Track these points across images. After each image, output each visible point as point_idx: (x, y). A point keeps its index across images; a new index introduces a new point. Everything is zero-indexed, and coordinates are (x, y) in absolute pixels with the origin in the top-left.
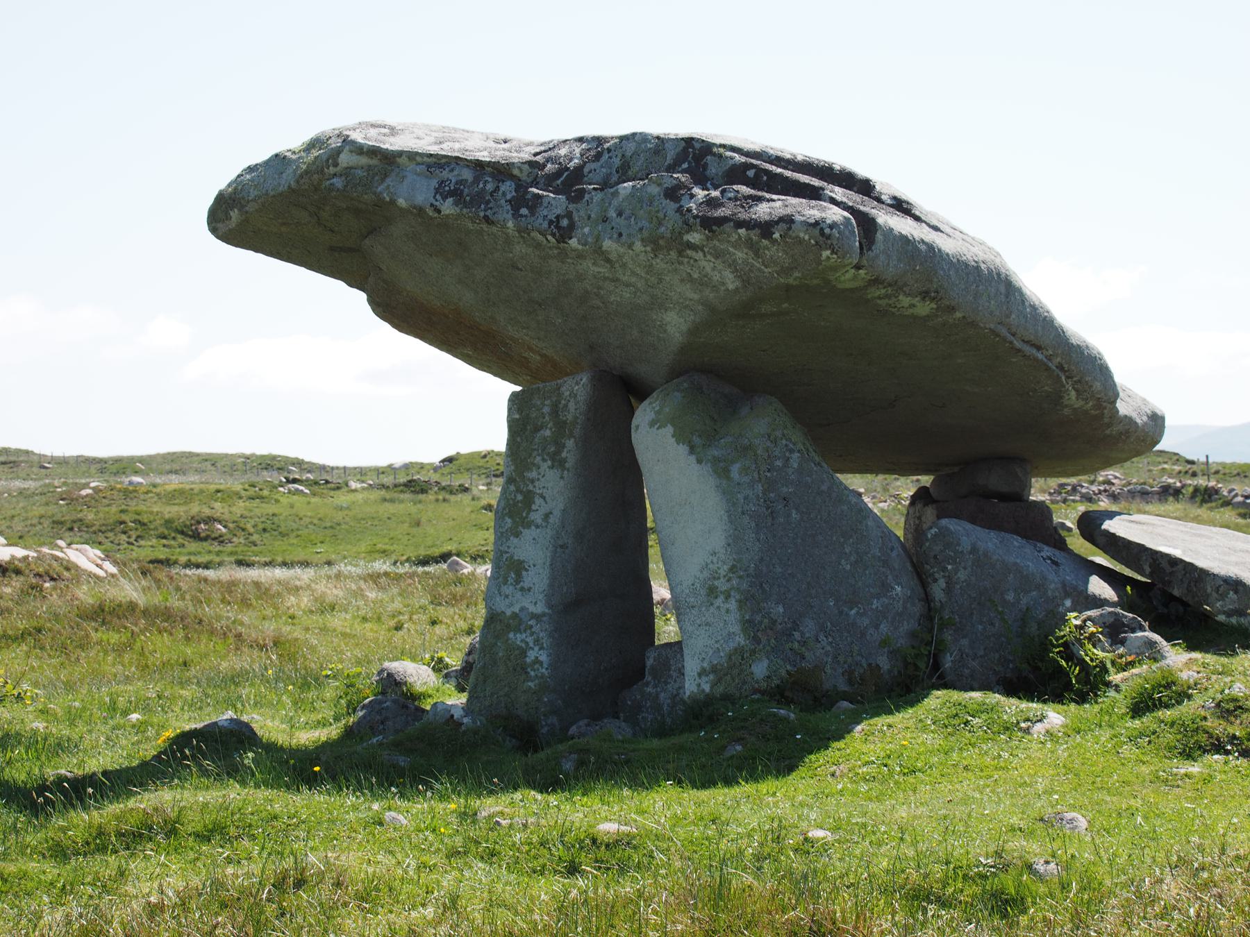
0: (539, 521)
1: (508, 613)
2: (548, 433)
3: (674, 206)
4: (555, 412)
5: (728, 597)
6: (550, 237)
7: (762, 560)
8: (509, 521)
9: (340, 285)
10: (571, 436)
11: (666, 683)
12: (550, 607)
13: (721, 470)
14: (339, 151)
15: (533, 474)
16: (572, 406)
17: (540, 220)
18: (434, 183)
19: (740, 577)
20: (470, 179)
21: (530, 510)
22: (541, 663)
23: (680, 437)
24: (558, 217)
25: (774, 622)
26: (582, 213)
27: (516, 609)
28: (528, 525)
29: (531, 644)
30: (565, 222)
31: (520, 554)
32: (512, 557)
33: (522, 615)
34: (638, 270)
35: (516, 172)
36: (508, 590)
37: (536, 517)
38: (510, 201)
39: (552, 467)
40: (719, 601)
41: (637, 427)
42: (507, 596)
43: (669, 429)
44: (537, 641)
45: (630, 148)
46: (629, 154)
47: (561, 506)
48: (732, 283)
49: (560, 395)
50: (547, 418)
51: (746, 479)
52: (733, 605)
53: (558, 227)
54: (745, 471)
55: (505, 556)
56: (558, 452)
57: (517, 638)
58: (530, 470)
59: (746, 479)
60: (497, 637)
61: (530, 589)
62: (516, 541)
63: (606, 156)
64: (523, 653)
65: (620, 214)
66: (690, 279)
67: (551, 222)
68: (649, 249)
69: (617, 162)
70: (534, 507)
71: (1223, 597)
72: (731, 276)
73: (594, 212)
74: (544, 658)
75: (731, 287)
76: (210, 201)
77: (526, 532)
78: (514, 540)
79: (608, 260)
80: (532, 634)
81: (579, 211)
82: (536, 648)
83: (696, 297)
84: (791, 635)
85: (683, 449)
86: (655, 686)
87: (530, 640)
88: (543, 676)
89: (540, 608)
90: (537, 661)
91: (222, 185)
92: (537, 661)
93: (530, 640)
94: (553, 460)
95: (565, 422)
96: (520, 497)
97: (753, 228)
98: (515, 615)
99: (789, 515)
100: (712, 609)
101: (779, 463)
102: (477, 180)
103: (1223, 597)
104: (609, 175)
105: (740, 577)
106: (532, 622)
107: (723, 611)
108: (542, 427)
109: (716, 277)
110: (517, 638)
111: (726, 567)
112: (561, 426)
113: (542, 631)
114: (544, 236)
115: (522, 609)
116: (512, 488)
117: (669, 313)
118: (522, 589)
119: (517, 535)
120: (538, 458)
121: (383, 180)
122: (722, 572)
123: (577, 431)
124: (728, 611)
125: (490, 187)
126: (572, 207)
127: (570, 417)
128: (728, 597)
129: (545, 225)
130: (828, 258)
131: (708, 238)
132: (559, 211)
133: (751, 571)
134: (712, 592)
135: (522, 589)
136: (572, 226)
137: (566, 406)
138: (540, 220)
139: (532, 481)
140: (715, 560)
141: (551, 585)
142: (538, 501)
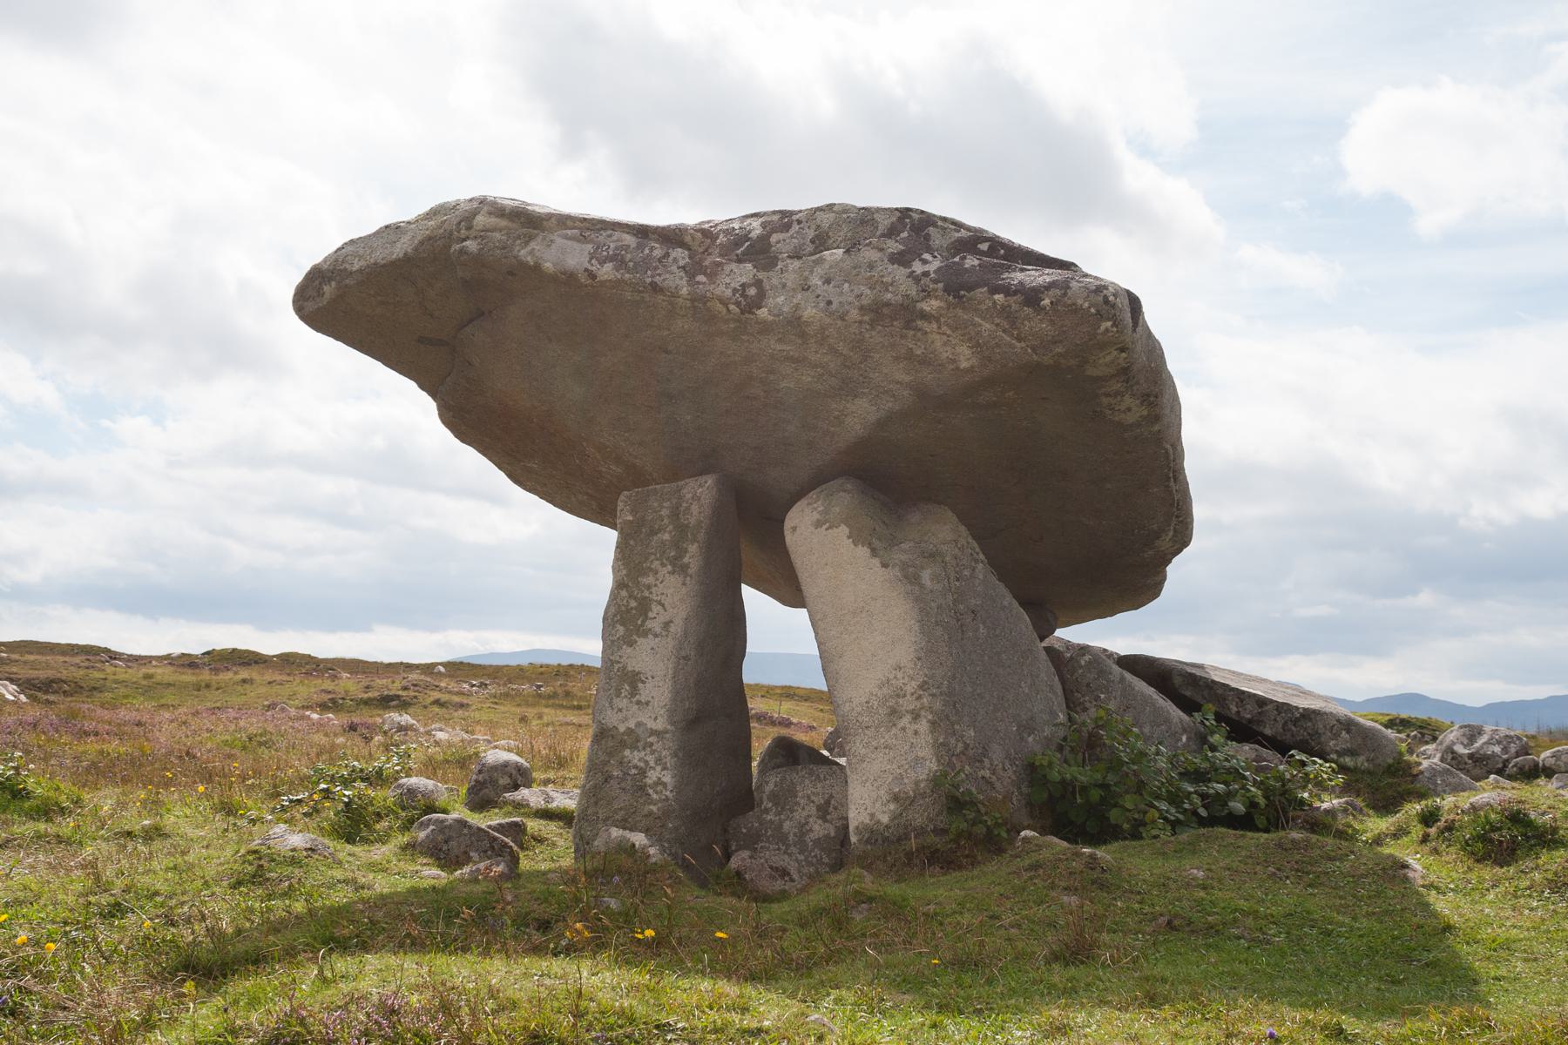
0: (658, 630)
1: (622, 729)
2: (666, 536)
3: (903, 271)
4: (675, 514)
5: (916, 717)
6: (732, 307)
7: (954, 677)
8: (621, 629)
9: (412, 385)
10: (694, 540)
11: (792, 811)
12: (672, 723)
13: (910, 577)
14: (475, 213)
15: (650, 580)
16: (695, 509)
17: (722, 287)
18: (589, 247)
19: (933, 695)
20: (633, 245)
21: (646, 618)
22: (665, 785)
23: (856, 537)
24: (743, 285)
25: (966, 746)
26: (775, 281)
28: (645, 634)
29: (652, 764)
30: (752, 291)
31: (633, 665)
32: (624, 668)
33: (640, 731)
34: (841, 347)
35: (688, 239)
36: (622, 703)
37: (655, 625)
38: (683, 268)
39: (672, 573)
40: (905, 721)
41: (794, 529)
42: (620, 710)
43: (844, 530)
44: (658, 760)
45: (826, 220)
46: (826, 225)
47: (683, 615)
48: (965, 357)
49: (680, 498)
50: (666, 521)
51: (938, 587)
52: (923, 726)
53: (743, 295)
54: (935, 578)
56: (679, 557)
57: (634, 757)
58: (645, 574)
59: (938, 587)
60: (610, 755)
61: (647, 703)
62: (629, 650)
63: (796, 227)
65: (828, 281)
66: (910, 356)
67: (735, 291)
68: (866, 318)
69: (811, 234)
70: (651, 615)
71: (1336, 736)
72: (968, 352)
73: (791, 278)
75: (964, 365)
76: (298, 278)
77: (640, 641)
79: (803, 335)
80: (653, 752)
81: (772, 279)
82: (659, 768)
83: (907, 378)
84: (981, 761)
85: (863, 551)
86: (779, 814)
87: (651, 759)
88: (667, 799)
89: (660, 725)
90: (659, 782)
91: (318, 259)
92: (659, 782)
93: (651, 759)
94: (674, 565)
95: (687, 526)
96: (633, 604)
97: (1015, 293)
98: (630, 731)
99: (977, 630)
100: (894, 731)
101: (966, 572)
102: (640, 247)
103: (1336, 736)
104: (801, 246)
105: (933, 695)
107: (910, 733)
108: (660, 530)
109: (946, 354)
110: (634, 757)
112: (682, 530)
113: (665, 749)
114: (726, 305)
115: (639, 724)
116: (624, 593)
117: (857, 401)
118: (638, 703)
119: (631, 644)
120: (657, 563)
121: (527, 243)
122: (909, 689)
123: (701, 536)
124: (916, 733)
125: (658, 253)
126: (761, 275)
127: (693, 521)
128: (916, 717)
129: (729, 293)
130: (1107, 330)
131: (949, 306)
132: (744, 280)
133: (944, 688)
134: (894, 712)
135: (638, 703)
136: (762, 294)
137: (688, 508)
138: (722, 287)
139: (649, 587)
140: (900, 675)
141: (674, 700)
142: (656, 608)
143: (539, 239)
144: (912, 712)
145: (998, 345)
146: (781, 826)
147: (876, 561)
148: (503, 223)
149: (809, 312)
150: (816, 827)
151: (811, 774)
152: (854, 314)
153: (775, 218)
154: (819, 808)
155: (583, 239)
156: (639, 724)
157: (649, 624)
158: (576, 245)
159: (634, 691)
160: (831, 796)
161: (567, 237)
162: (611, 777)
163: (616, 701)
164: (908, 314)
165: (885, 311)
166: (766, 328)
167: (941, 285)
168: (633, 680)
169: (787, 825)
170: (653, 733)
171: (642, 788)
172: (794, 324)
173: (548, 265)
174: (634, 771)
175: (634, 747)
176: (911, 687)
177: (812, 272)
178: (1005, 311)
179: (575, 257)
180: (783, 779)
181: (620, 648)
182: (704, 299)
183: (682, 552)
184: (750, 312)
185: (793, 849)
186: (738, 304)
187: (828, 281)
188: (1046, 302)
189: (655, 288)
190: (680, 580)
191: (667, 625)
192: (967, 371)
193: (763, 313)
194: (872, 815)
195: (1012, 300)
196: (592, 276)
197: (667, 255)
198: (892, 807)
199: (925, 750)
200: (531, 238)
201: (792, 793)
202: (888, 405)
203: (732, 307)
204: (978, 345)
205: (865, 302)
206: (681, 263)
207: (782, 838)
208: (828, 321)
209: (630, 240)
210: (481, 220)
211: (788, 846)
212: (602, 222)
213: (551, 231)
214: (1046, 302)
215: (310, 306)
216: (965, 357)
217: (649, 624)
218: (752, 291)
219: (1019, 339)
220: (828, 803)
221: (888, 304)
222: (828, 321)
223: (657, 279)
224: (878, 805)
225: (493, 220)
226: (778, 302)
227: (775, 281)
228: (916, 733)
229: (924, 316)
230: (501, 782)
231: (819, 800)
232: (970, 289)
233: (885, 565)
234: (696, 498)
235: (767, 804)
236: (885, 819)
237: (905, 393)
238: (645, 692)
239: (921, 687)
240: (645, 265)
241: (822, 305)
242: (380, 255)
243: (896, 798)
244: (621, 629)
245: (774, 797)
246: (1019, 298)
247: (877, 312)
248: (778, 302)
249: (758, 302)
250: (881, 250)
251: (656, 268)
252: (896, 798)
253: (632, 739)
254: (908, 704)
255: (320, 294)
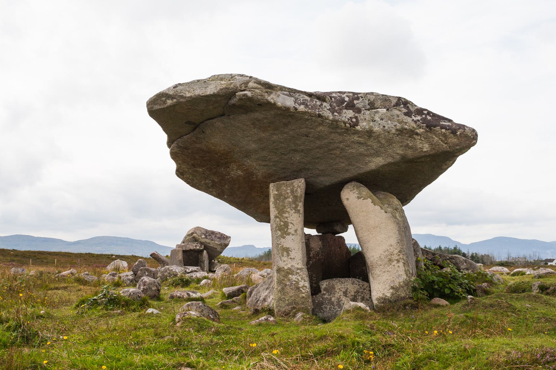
0: (293, 233)
1: (286, 268)
2: (290, 200)
4: (292, 192)
5: (398, 261)
10: (300, 201)
11: (334, 294)
15: (286, 215)
16: (299, 190)
21: (288, 229)
22: (306, 287)
27: (289, 266)
29: (300, 279)
33: (293, 268)
36: (285, 258)
38: (329, 109)
41: (348, 199)
44: (302, 278)
45: (372, 98)
49: (294, 186)
50: (290, 194)
52: (401, 264)
55: (280, 246)
57: (293, 278)
62: (284, 240)
63: (361, 99)
64: (297, 283)
74: (307, 284)
75: (425, 150)
77: (287, 237)
78: (282, 240)
80: (300, 276)
81: (361, 116)
82: (303, 281)
83: (401, 152)
85: (377, 207)
87: (299, 278)
89: (300, 266)
92: (304, 286)
93: (299, 278)
94: (295, 210)
95: (297, 196)
96: (282, 223)
97: (449, 129)
98: (289, 269)
100: (391, 266)
106: (298, 271)
107: (396, 266)
111: (397, 251)
112: (296, 197)
113: (304, 274)
115: (292, 266)
116: (278, 220)
118: (291, 258)
119: (284, 238)
123: (303, 200)
124: (399, 266)
126: (357, 115)
127: (299, 195)
128: (398, 261)
129: (347, 120)
131: (426, 131)
135: (291, 258)
137: (296, 190)
139: (287, 218)
142: (290, 225)
143: (274, 94)
144: (397, 260)
145: (438, 145)
146: (331, 299)
147: (383, 211)
148: (259, 86)
149: (376, 129)
150: (343, 299)
151: (340, 281)
152: (394, 131)
153: (351, 95)
154: (344, 293)
155: (290, 96)
156: (292, 266)
157: (289, 231)
158: (288, 97)
159: (288, 255)
160: (347, 288)
161: (284, 94)
162: (286, 285)
163: (283, 258)
164: (412, 133)
165: (404, 131)
166: (357, 132)
167: (425, 125)
168: (287, 250)
169: (333, 299)
170: (298, 269)
171: (298, 288)
172: (370, 133)
173: (279, 103)
174: (294, 283)
175: (293, 274)
176: (396, 252)
177: (375, 115)
178: (444, 135)
179: (289, 102)
180: (329, 283)
181: (280, 239)
182: (337, 121)
183: (297, 206)
184: (354, 127)
185: (336, 307)
186: (350, 124)
187: (382, 119)
188: (459, 133)
189: (320, 116)
190: (298, 215)
191: (296, 231)
192: (425, 152)
193: (358, 128)
194: (383, 294)
195: (447, 131)
196: (296, 109)
197: (322, 104)
198: (391, 291)
199: (402, 273)
200: (271, 93)
201: (334, 288)
202: (390, 160)
203: (347, 125)
204: (432, 144)
205: (398, 128)
206: (328, 108)
207: (332, 303)
208: (383, 132)
209: (307, 98)
210: (251, 84)
211: (334, 306)
212: (295, 90)
213: (277, 91)
214: (459, 133)
215: (157, 107)
216: (426, 147)
217: (289, 231)
218: (354, 120)
219: (446, 144)
220: (347, 291)
221: (406, 129)
222: (383, 132)
223: (320, 113)
224: (385, 290)
225: (256, 85)
226: (363, 125)
227: (362, 117)
228: (399, 266)
229: (417, 134)
230: (153, 289)
231: (344, 290)
232: (435, 127)
233: (386, 212)
234: (299, 186)
235: (323, 292)
236: (389, 295)
237: (398, 157)
238: (292, 254)
239: (399, 252)
240: (314, 107)
241: (381, 127)
242: (199, 92)
243: (392, 288)
244: (279, 233)
245: (325, 289)
246: (450, 131)
247: (401, 132)
248: (363, 125)
249: (357, 124)
250: (400, 111)
251: (319, 109)
252: (392, 288)
253: (290, 272)
254: (395, 257)
255: (165, 102)
